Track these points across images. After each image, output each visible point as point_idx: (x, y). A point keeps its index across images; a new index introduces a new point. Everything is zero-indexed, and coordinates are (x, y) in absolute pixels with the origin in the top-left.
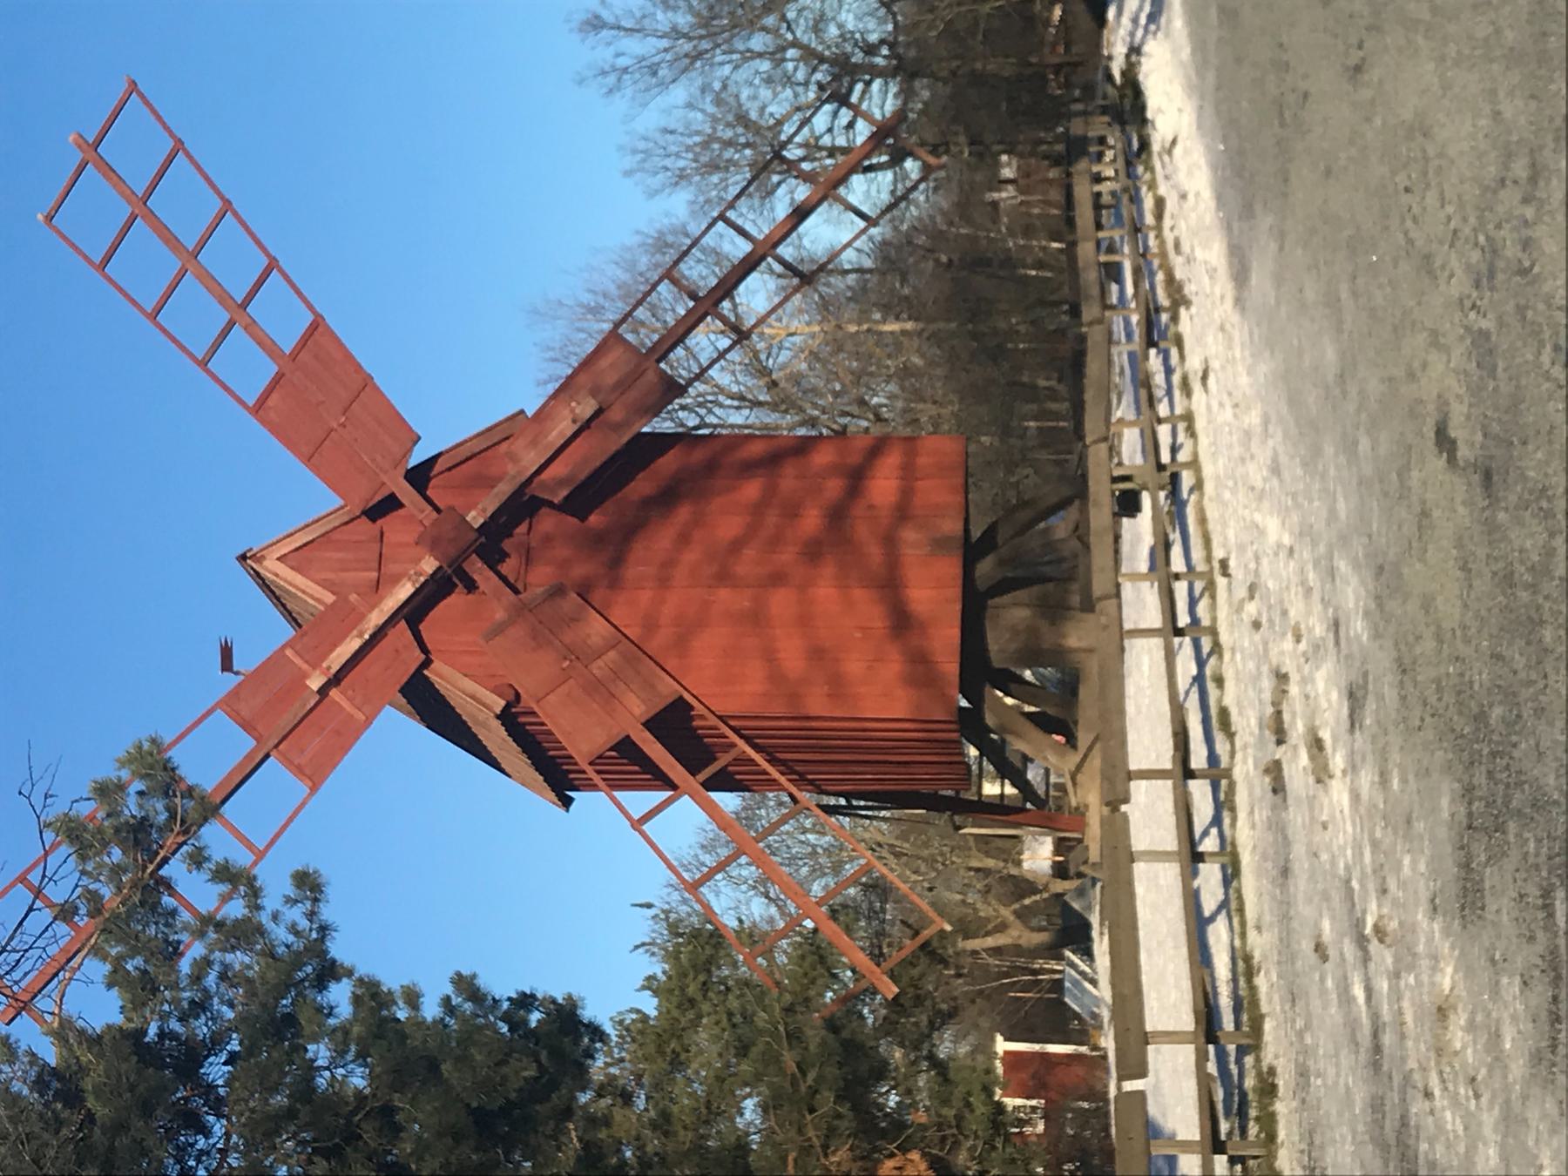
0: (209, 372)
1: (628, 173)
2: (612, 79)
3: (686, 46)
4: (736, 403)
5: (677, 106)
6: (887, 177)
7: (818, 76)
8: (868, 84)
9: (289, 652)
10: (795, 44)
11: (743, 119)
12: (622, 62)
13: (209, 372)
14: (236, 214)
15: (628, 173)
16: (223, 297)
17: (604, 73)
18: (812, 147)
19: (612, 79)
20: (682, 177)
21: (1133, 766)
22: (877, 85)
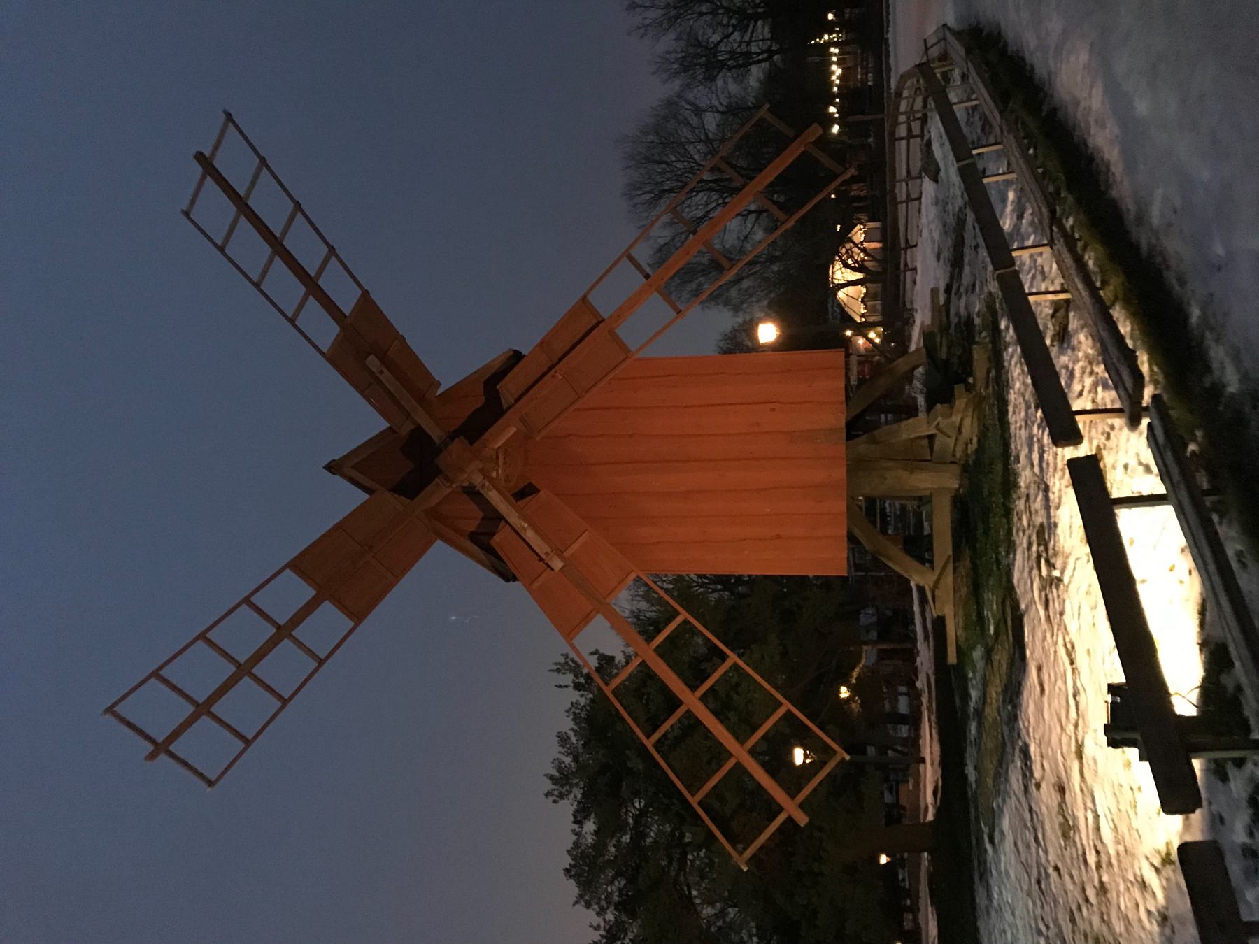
0: (328, 657)
1: (654, 73)
2: (642, 31)
3: (673, 13)
4: (1036, 447)
5: (668, 42)
6: (765, 65)
7: (734, 21)
8: (756, 22)
9: (535, 586)
10: (722, 7)
11: (698, 44)
12: (648, 22)
13: (328, 657)
14: (161, 668)
15: (654, 73)
16: (272, 643)
17: (639, 28)
18: (732, 53)
19: (642, 31)
20: (676, 74)
21: (1115, 494)
22: (760, 23)
